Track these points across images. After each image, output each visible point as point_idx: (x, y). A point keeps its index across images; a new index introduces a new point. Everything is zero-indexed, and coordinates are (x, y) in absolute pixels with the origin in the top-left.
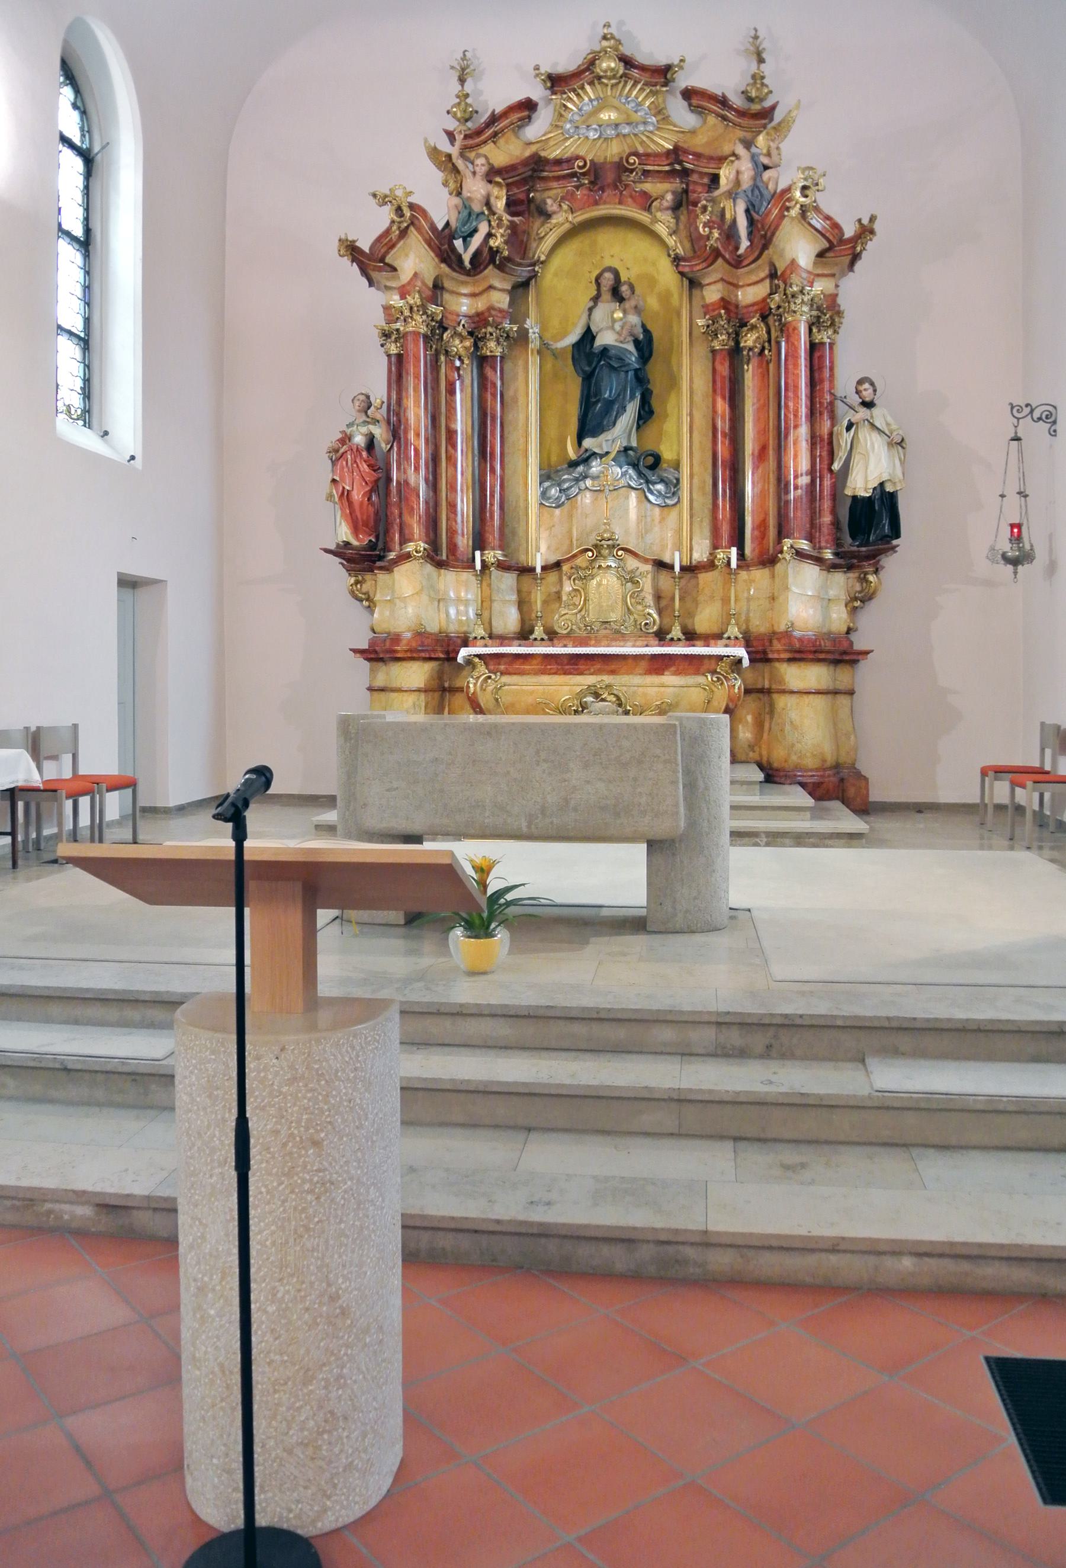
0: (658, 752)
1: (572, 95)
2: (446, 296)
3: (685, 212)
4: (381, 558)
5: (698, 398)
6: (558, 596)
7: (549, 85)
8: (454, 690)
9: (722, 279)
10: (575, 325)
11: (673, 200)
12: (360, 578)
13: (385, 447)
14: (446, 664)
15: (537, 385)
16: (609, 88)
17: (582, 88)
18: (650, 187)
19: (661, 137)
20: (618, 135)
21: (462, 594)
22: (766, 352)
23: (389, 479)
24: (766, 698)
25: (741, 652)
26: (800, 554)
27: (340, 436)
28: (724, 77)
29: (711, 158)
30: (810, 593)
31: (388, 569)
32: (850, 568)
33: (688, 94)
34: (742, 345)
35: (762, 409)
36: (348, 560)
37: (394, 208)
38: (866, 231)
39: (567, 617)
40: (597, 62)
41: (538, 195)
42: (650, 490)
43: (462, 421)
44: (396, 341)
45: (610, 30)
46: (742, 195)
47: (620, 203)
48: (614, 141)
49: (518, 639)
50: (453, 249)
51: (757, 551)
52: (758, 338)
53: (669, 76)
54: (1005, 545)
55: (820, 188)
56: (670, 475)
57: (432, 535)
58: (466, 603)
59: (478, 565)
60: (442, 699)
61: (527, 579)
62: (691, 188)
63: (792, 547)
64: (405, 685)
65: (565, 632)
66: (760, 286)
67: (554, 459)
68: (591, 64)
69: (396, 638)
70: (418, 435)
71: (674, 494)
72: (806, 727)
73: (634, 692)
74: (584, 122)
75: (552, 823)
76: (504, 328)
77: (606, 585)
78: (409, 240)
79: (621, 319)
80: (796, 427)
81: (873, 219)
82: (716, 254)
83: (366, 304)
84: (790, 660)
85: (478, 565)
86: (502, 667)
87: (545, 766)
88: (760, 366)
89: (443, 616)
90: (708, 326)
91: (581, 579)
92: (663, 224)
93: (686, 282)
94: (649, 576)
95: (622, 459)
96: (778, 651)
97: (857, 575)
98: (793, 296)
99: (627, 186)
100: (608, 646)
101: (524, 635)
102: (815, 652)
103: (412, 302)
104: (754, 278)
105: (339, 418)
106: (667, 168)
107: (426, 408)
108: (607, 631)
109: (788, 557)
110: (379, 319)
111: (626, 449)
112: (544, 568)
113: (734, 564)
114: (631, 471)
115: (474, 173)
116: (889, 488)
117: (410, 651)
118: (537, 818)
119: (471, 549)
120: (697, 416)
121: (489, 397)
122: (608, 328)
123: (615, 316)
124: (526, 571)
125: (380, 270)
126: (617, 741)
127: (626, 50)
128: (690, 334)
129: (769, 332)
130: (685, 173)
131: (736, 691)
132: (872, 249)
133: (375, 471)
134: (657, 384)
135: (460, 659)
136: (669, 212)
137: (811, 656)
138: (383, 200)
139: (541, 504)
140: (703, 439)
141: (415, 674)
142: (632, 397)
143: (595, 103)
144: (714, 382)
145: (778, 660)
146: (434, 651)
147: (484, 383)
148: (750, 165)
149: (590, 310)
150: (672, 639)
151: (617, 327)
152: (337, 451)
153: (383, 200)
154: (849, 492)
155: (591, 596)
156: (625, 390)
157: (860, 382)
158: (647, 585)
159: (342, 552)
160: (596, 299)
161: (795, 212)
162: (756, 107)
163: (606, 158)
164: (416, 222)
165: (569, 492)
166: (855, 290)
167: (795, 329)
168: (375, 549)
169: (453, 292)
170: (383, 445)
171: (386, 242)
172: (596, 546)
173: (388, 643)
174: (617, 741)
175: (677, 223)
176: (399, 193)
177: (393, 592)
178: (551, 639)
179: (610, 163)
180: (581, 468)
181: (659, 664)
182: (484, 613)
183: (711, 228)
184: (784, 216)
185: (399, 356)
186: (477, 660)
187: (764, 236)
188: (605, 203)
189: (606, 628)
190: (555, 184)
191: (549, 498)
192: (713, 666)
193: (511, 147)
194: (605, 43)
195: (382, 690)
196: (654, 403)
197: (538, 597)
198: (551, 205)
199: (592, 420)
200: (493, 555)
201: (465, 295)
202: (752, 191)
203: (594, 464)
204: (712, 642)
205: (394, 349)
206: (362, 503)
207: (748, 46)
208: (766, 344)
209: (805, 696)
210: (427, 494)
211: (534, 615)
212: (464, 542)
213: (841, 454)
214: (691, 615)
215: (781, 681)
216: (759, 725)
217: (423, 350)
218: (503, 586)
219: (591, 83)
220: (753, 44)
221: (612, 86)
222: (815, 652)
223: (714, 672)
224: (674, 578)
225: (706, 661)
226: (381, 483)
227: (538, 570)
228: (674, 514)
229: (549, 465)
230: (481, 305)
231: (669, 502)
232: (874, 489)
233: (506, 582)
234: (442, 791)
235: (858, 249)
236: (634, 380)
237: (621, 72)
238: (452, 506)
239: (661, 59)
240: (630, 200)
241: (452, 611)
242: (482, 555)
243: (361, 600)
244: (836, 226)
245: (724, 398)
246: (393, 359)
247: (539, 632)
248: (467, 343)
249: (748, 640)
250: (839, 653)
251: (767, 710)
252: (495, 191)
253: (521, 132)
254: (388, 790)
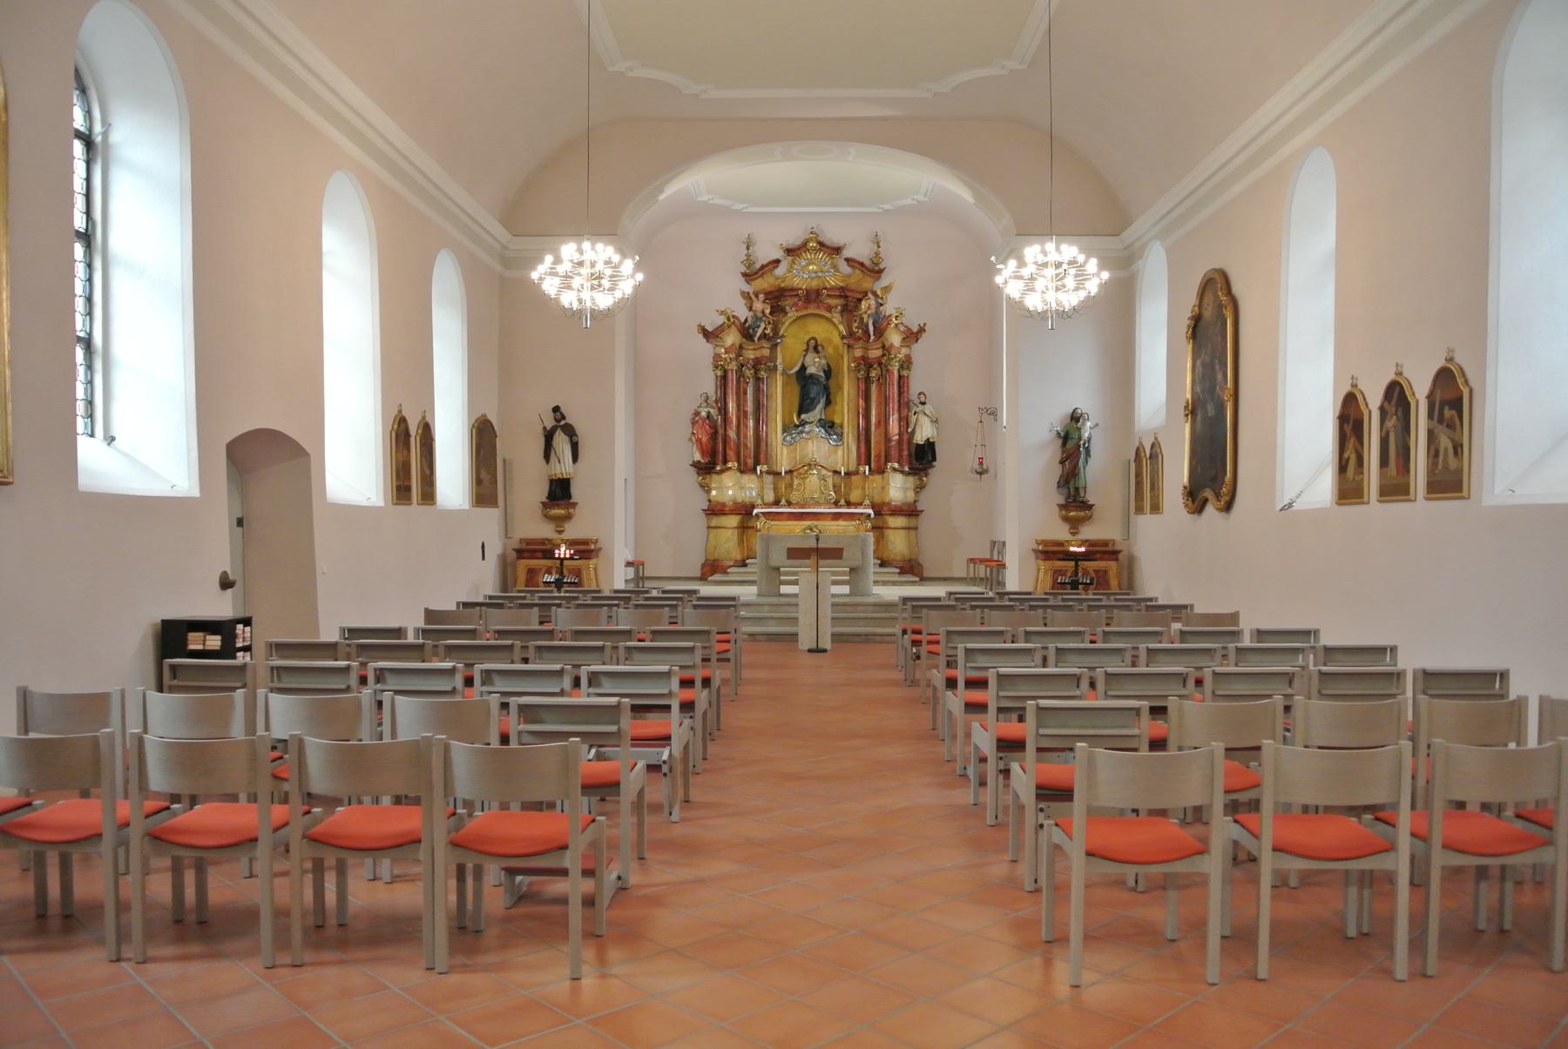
25: (871, 511)
26: (894, 470)
28: (860, 250)
33: (847, 260)
35: (878, 406)
38: (922, 330)
43: (750, 407)
54: (977, 466)
68: (805, 244)
69: (724, 505)
72: (898, 543)
77: (813, 480)
83: (706, 349)
92: (837, 318)
101: (777, 503)
138: (722, 313)
141: (733, 521)
153: (722, 313)
158: (830, 481)
159: (696, 465)
166: (919, 350)
181: (836, 516)
182: (761, 495)
214: (848, 494)
230: (758, 354)
233: (769, 479)
249: (873, 506)
250: (911, 511)
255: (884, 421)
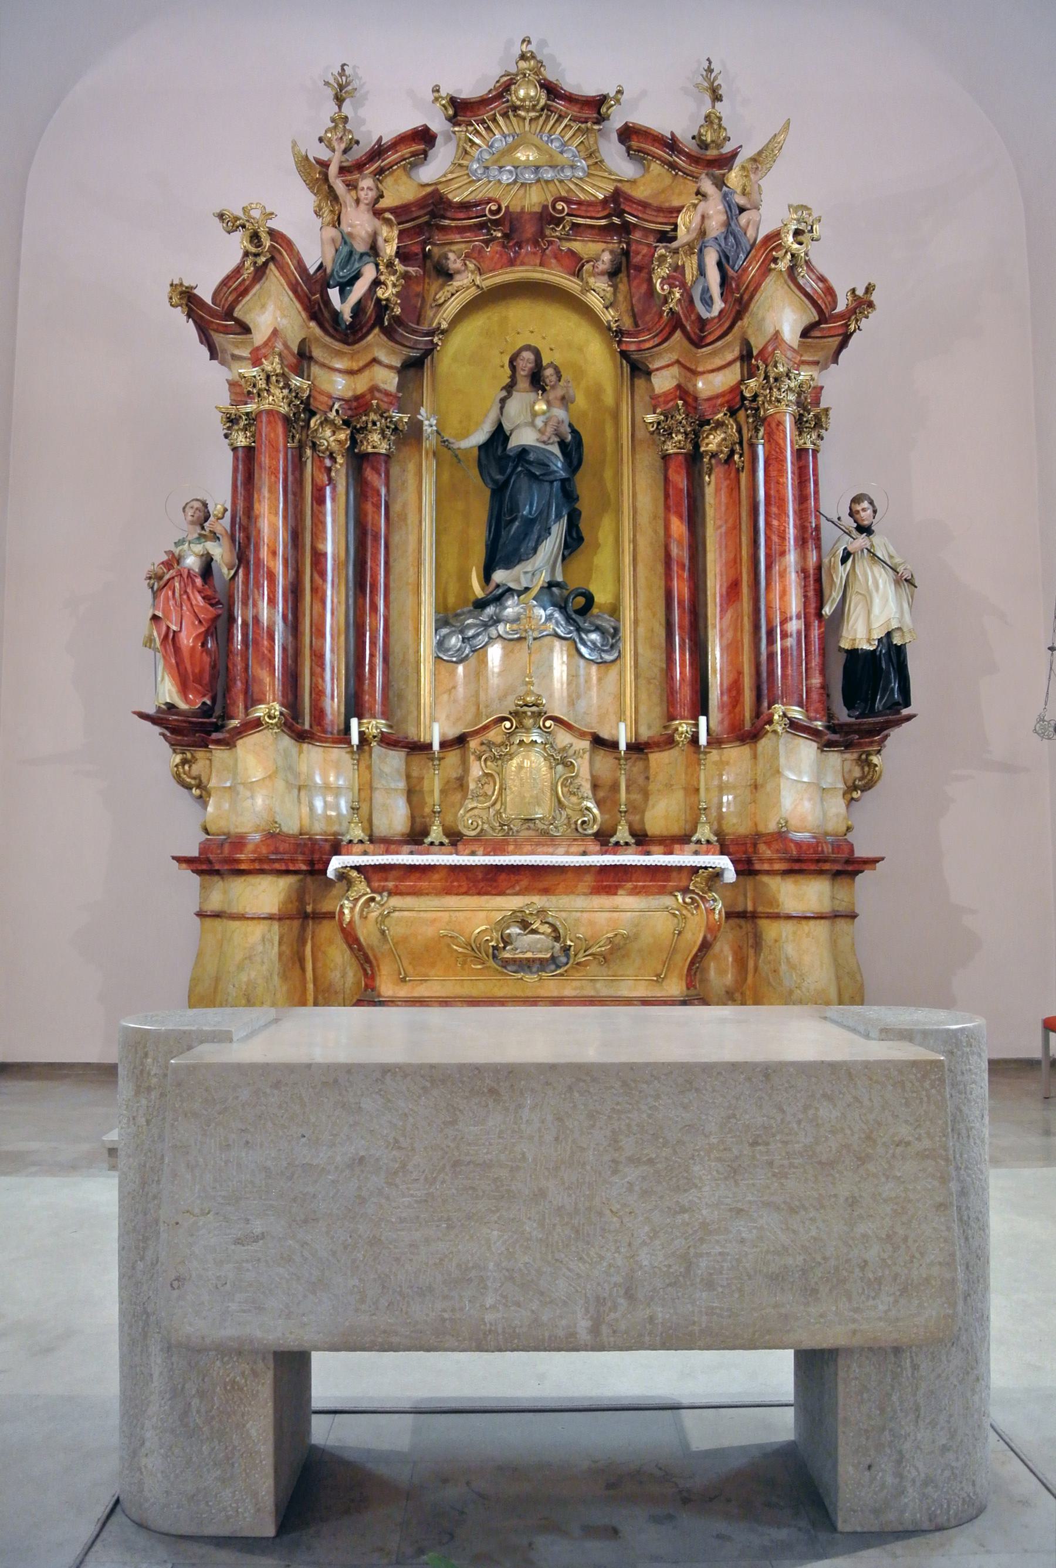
0: (904, 1131)
1: (481, 128)
2: (315, 369)
3: (625, 280)
4: (218, 728)
5: (644, 519)
6: (461, 783)
7: (451, 112)
8: (319, 917)
9: (678, 362)
10: (478, 425)
11: (612, 261)
12: (189, 756)
13: (227, 573)
14: (309, 879)
15: (433, 497)
16: (527, 122)
17: (494, 120)
18: (582, 247)
19: (593, 186)
20: (538, 181)
21: (332, 779)
22: (736, 457)
23: (232, 619)
24: (747, 926)
27: (165, 558)
28: (674, 116)
29: (660, 210)
30: (805, 779)
31: (229, 743)
32: (848, 746)
33: (628, 134)
34: (702, 449)
36: (173, 731)
37: (248, 233)
38: (862, 304)
39: (476, 812)
40: (513, 87)
41: (436, 250)
42: (582, 640)
43: (333, 543)
44: (245, 429)
45: (531, 48)
46: (711, 243)
47: (541, 265)
48: (534, 188)
49: (407, 843)
50: (327, 302)
51: (726, 723)
52: (724, 439)
53: (603, 110)
55: (815, 235)
56: (607, 624)
57: (290, 697)
58: (337, 791)
59: (355, 739)
60: (303, 928)
61: (418, 759)
62: (633, 247)
63: (785, 715)
64: (251, 910)
65: (473, 833)
66: (727, 371)
67: (451, 600)
68: (506, 88)
69: (238, 842)
70: (274, 553)
71: (612, 646)
73: (577, 920)
74: (495, 162)
75: (651, 1319)
76: (391, 417)
77: (529, 767)
78: (267, 283)
79: (544, 413)
80: (783, 553)
81: (869, 289)
82: (675, 323)
83: (206, 383)
84: (787, 873)
85: (355, 739)
86: (390, 884)
87: (632, 1174)
88: (727, 474)
89: (305, 810)
90: (659, 423)
91: (495, 759)
92: (597, 293)
93: (627, 368)
94: (587, 756)
95: (546, 598)
96: (770, 860)
97: (855, 756)
98: (776, 380)
99: (550, 243)
100: (533, 853)
101: (416, 837)
102: (818, 861)
103: (269, 368)
104: (718, 362)
105: (166, 534)
106: (603, 222)
107: (285, 517)
108: (531, 833)
109: (779, 729)
110: (224, 398)
111: (551, 585)
112: (443, 745)
113: (703, 740)
114: (557, 615)
115: (358, 201)
116: (897, 640)
117: (260, 860)
118: (614, 1308)
119: (342, 717)
120: (643, 542)
121: (369, 507)
122: (526, 424)
123: (537, 407)
124: (418, 748)
125: (226, 330)
126: (806, 1108)
127: (550, 75)
128: (633, 435)
129: (739, 431)
130: (626, 229)
131: (717, 917)
132: (868, 327)
133: (212, 605)
134: (585, 505)
135: (330, 873)
136: (605, 278)
137: (813, 867)
138: (231, 223)
139: (438, 657)
140: (650, 575)
141: (266, 894)
142: (559, 517)
143: (510, 139)
144: (667, 496)
145: (768, 873)
146: (293, 861)
147: (362, 491)
148: (721, 207)
149: (503, 401)
150: (617, 843)
151: (539, 422)
152: (160, 578)
153: (231, 223)
154: (845, 645)
155: (509, 783)
156: (549, 506)
157: (857, 500)
158: (583, 766)
159: (164, 719)
160: (510, 388)
161: (783, 265)
162: (712, 153)
163: (523, 208)
164: (278, 257)
165: (476, 641)
166: (838, 384)
167: (779, 423)
168: (210, 716)
169: (323, 365)
170: (225, 570)
171: (236, 287)
172: (515, 714)
173: (227, 849)
174: (806, 1108)
175: (615, 293)
176: (256, 214)
177: (235, 774)
178: (454, 844)
179: (530, 213)
180: (490, 610)
181: (609, 880)
182: (362, 807)
183: (672, 286)
184: (770, 270)
185: (249, 450)
186: (354, 874)
187: (739, 301)
188: (523, 264)
189: (529, 829)
190: (458, 238)
191: (448, 650)
192: (684, 884)
193: (402, 189)
194: (523, 64)
195: (217, 915)
196: (583, 526)
197: (434, 782)
198: (454, 262)
199: (500, 553)
200: (375, 725)
201: (339, 371)
202: (726, 238)
203: (509, 603)
204: (677, 847)
205: (241, 440)
206: (193, 649)
207: (700, 79)
208: (737, 447)
209: (804, 922)
210: (285, 638)
211: (427, 810)
212: (334, 705)
213: (834, 594)
214: (635, 809)
215: (773, 901)
216: (741, 963)
217: (278, 441)
218: (387, 769)
219: (505, 115)
220: (706, 78)
221: (531, 120)
222: (818, 861)
223: (685, 891)
224: (619, 759)
225: (674, 874)
226: (219, 625)
227: (436, 747)
228: (613, 672)
229: (446, 608)
230: (361, 384)
231: (608, 657)
232: (880, 640)
234: (374, 1242)
235: (852, 327)
236: (560, 495)
237: (542, 102)
238: (318, 657)
239: (590, 89)
240: (553, 261)
241: (319, 804)
242: (360, 724)
243: (189, 787)
244: (830, 291)
245: (681, 517)
246: (240, 453)
247: (436, 833)
248: (342, 436)
250: (836, 861)
251: (751, 941)
252: (384, 231)
253: (413, 174)
254: (238, 1242)
255: (748, 586)
